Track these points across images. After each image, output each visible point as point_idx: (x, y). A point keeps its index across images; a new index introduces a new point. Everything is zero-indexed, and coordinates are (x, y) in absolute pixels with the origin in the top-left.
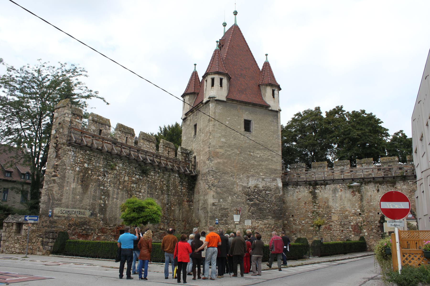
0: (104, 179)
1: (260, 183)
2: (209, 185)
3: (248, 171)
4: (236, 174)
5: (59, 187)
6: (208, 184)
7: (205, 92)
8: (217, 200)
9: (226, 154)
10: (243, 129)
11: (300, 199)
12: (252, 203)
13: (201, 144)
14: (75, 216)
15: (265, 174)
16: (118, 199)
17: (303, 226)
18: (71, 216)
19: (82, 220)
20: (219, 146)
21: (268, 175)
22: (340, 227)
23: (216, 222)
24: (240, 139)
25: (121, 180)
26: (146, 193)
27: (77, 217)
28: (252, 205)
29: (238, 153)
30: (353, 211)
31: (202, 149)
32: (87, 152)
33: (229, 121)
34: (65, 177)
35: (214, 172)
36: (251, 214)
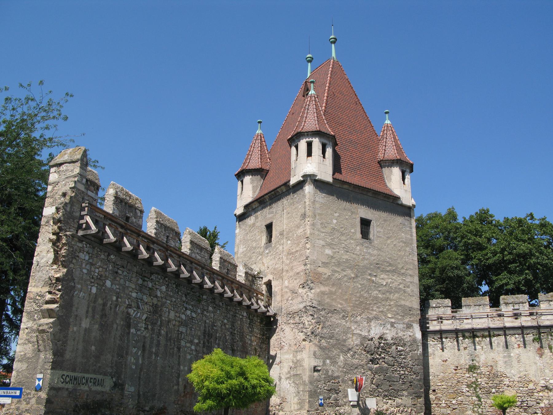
0: (137, 314)
1: (388, 331)
2: (306, 333)
3: (368, 309)
4: (350, 314)
5: (61, 325)
6: (304, 330)
7: (293, 166)
8: (322, 361)
9: (334, 277)
10: (359, 235)
11: (446, 361)
12: (376, 368)
13: (285, 258)
14: (86, 388)
15: (395, 315)
16: (158, 356)
17: (454, 409)
18: (79, 388)
19: (98, 397)
20: (323, 263)
21: (400, 317)
22: (521, 410)
23: (320, 401)
24: (355, 253)
25: (163, 318)
26: (201, 345)
27: (90, 389)
28: (375, 372)
29: (353, 276)
30: (543, 382)
31: (286, 268)
32: (112, 257)
33: (336, 219)
34: (72, 306)
35: (315, 309)
36: (375, 387)
